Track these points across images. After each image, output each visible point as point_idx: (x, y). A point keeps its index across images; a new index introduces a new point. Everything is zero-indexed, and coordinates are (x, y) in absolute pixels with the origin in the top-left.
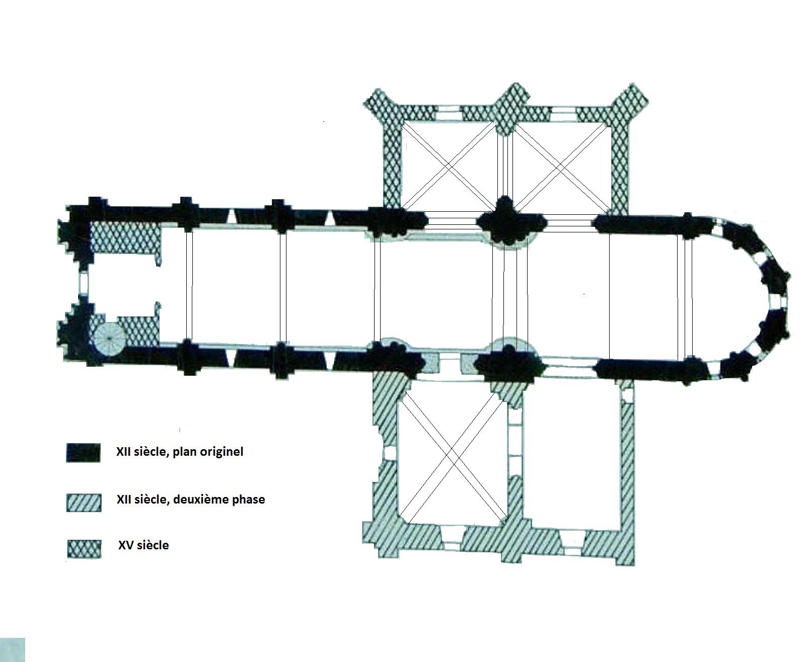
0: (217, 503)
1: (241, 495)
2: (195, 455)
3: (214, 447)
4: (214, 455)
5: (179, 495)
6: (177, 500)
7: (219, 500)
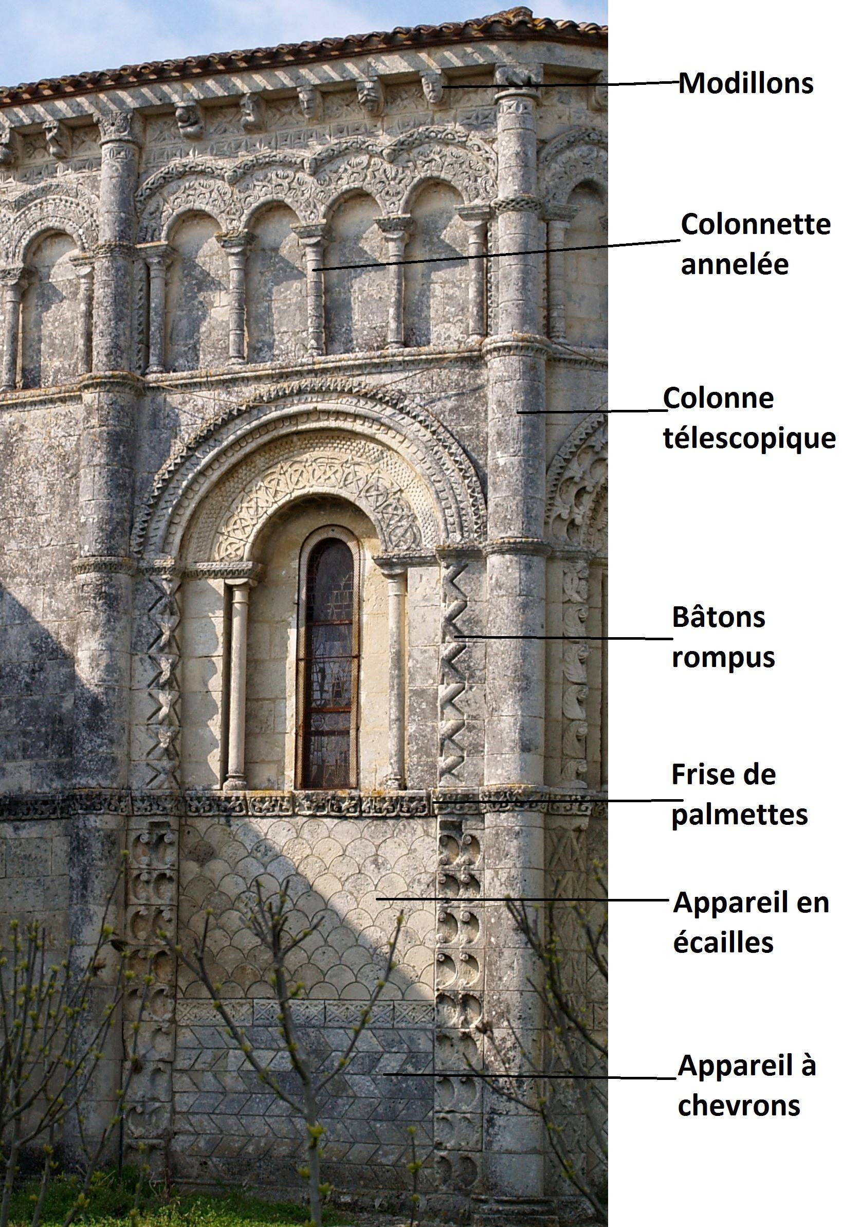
0: (714, 665)
1: (799, 452)
2: (826, 910)
3: (702, 765)
4: (723, 665)
5: (756, 764)
6: (751, 776)
7: (731, 815)
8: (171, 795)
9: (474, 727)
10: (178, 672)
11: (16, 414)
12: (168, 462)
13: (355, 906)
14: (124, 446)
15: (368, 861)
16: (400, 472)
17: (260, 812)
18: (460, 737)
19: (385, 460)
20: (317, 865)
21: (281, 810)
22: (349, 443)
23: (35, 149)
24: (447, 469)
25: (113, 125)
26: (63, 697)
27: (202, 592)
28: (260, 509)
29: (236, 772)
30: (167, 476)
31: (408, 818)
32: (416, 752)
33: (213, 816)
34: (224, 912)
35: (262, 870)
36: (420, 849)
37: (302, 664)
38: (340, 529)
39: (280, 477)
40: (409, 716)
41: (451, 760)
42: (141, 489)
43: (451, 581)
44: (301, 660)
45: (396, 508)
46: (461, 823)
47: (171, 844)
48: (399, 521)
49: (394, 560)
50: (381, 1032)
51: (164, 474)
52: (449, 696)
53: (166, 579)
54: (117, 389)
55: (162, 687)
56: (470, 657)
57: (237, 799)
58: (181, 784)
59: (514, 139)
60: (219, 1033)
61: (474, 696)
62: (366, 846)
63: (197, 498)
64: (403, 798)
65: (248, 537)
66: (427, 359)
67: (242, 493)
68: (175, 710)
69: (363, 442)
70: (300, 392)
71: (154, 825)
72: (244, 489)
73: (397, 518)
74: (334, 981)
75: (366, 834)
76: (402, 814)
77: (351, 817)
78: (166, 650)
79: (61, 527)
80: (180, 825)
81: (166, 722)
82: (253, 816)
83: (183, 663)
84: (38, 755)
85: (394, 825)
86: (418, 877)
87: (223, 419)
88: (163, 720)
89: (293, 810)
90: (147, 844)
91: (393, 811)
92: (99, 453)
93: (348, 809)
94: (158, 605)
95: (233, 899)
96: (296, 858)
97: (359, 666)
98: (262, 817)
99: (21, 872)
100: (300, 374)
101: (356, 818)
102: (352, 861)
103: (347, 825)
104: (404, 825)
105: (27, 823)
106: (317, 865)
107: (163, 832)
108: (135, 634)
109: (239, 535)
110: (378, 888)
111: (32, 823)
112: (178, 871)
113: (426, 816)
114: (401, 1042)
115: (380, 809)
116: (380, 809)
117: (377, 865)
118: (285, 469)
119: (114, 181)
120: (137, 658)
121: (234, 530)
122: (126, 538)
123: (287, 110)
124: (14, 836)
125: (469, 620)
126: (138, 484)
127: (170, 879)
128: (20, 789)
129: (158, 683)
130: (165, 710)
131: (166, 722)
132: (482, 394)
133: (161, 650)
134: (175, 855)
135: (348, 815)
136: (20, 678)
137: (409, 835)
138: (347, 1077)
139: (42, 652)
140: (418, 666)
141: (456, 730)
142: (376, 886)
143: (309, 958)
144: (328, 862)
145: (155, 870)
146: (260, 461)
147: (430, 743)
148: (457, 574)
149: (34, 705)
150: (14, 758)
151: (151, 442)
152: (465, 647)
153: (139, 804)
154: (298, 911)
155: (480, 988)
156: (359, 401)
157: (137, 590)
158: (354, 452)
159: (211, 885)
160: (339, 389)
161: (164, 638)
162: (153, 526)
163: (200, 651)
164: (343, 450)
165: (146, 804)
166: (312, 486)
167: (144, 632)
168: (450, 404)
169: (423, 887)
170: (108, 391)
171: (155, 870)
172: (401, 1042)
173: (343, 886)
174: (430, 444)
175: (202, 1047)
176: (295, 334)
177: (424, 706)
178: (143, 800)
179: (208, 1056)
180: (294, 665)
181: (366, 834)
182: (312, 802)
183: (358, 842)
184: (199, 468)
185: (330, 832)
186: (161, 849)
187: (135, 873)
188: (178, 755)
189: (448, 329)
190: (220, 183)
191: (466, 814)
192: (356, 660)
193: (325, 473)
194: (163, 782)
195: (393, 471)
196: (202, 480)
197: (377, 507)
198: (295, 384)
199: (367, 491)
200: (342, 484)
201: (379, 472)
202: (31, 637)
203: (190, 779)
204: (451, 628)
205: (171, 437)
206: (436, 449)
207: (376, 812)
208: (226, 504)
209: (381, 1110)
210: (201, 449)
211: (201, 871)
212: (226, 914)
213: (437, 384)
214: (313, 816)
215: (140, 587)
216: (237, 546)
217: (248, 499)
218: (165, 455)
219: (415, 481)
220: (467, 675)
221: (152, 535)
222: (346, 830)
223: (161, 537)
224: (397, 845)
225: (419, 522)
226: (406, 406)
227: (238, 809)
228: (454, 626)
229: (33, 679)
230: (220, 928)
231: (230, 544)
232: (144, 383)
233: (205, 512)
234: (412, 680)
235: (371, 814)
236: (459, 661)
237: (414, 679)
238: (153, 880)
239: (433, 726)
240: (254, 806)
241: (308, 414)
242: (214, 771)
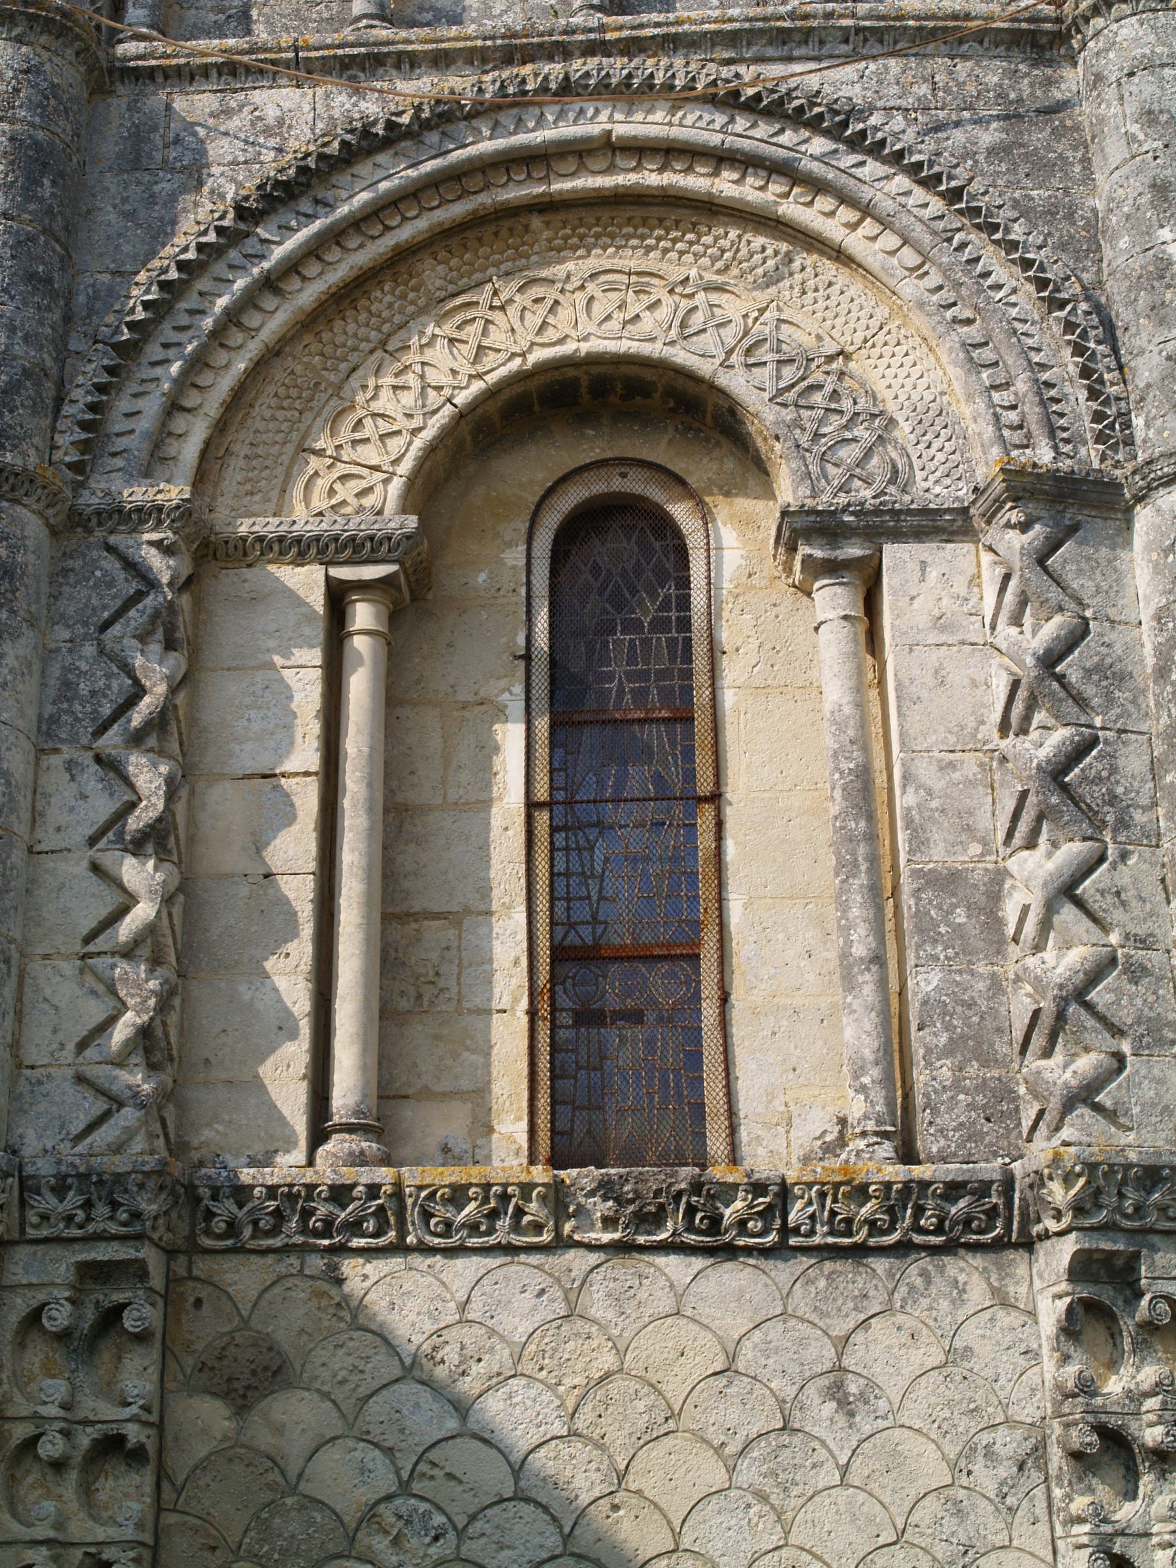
8: (161, 1171)
9: (1144, 969)
10: (180, 808)
12: (180, 241)
13: (775, 1539)
14: (54, 183)
15: (811, 1390)
16: (844, 307)
17: (446, 1234)
18: (1110, 997)
19: (798, 277)
20: (641, 1405)
21: (516, 1228)
22: (690, 236)
24: (999, 287)
27: (256, 599)
28: (432, 393)
29: (357, 1113)
30: (173, 274)
31: (934, 1250)
32: (949, 1051)
33: (287, 1249)
35: (452, 1424)
36: (984, 1350)
38: (646, 473)
39: (491, 315)
40: (919, 946)
41: (1086, 1064)
42: (91, 312)
43: (1041, 561)
44: (540, 805)
45: (835, 395)
46: (1136, 1256)
47: (142, 1338)
48: (846, 427)
49: (847, 518)
51: (164, 271)
52: (1067, 873)
53: (158, 544)
54: (44, 39)
55: (137, 847)
56: (1113, 770)
57: (373, 1190)
58: (178, 1148)
61: (1136, 881)
62: (802, 1342)
63: (254, 348)
64: (924, 1185)
65: (396, 462)
66: (920, 29)
67: (379, 354)
68: (170, 915)
69: (733, 234)
70: (567, 89)
72: (383, 344)
73: (836, 421)
75: (801, 1301)
76: (918, 1239)
77: (749, 1251)
78: (152, 741)
80: (171, 1280)
81: (145, 951)
82: (425, 1249)
83: (192, 793)
85: (890, 1274)
86: (986, 1438)
87: (344, 143)
88: (137, 942)
89: (558, 1229)
90: (64, 1336)
91: (891, 1229)
93: (742, 1224)
94: (132, 613)
95: (350, 1520)
96: (568, 1382)
97: (720, 825)
98: (450, 1252)
100: (561, 51)
101: (765, 1252)
102: (759, 1390)
104: (924, 1273)
106: (641, 1405)
107: (119, 1297)
108: (52, 692)
109: (370, 454)
110: (854, 1478)
112: (160, 1426)
113: (999, 1245)
115: (849, 1221)
116: (849, 1221)
118: (504, 296)
120: (56, 760)
121: (355, 443)
122: (46, 423)
125: (1098, 668)
126: (82, 299)
127: (137, 1456)
129: (121, 835)
130: (143, 912)
131: (145, 951)
132: (1069, 123)
133: (136, 739)
134: (153, 1373)
135: (741, 1242)
137: (945, 1305)
140: (934, 804)
141: (1094, 976)
142: (845, 1470)
144: (675, 1391)
145: (86, 1423)
146: (433, 274)
147: (989, 1024)
148: (1053, 546)
151: (125, 200)
152: (1095, 741)
153: (48, 1202)
154: (580, 1557)
156: (732, 120)
157: (65, 572)
158: (705, 261)
159: (275, 1476)
160: (679, 83)
161: (146, 706)
162: (124, 404)
163: (248, 759)
164: (673, 255)
165: (73, 1199)
166: (585, 339)
167: (84, 688)
168: (989, 137)
169: (1005, 1471)
170: (19, 40)
171: (86, 1423)
173: (731, 1470)
174: (941, 225)
177: (960, 916)
178: (60, 1190)
180: (520, 820)
182: (620, 1201)
183: (775, 1330)
184: (266, 265)
185: (679, 1298)
186: (106, 1356)
187: (20, 1432)
188: (171, 1059)
191: (1152, 1231)
192: (708, 810)
193: (622, 306)
194: (130, 1134)
195: (821, 304)
196: (180, 423)
197: (781, 392)
199: (748, 352)
200: (673, 333)
201: (779, 309)
203: (207, 1134)
204: (1055, 685)
205: (184, 189)
206: (958, 238)
207: (831, 1233)
208: (332, 377)
210: (275, 220)
211: (240, 1430)
213: (947, 90)
214: (623, 1248)
215: (77, 564)
216: (364, 484)
217: (398, 366)
218: (164, 230)
219: (892, 326)
220: (1110, 818)
221: (117, 428)
223: (146, 435)
224: (904, 1337)
225: (904, 431)
226: (876, 129)
227: (370, 1225)
228: (1061, 679)
231: (343, 478)
232: (113, 59)
233: (271, 389)
234: (919, 843)
235: (817, 1240)
236: (1084, 779)
237: (925, 842)
238: (78, 1458)
239: (994, 975)
240: (427, 1215)
242: (286, 1112)
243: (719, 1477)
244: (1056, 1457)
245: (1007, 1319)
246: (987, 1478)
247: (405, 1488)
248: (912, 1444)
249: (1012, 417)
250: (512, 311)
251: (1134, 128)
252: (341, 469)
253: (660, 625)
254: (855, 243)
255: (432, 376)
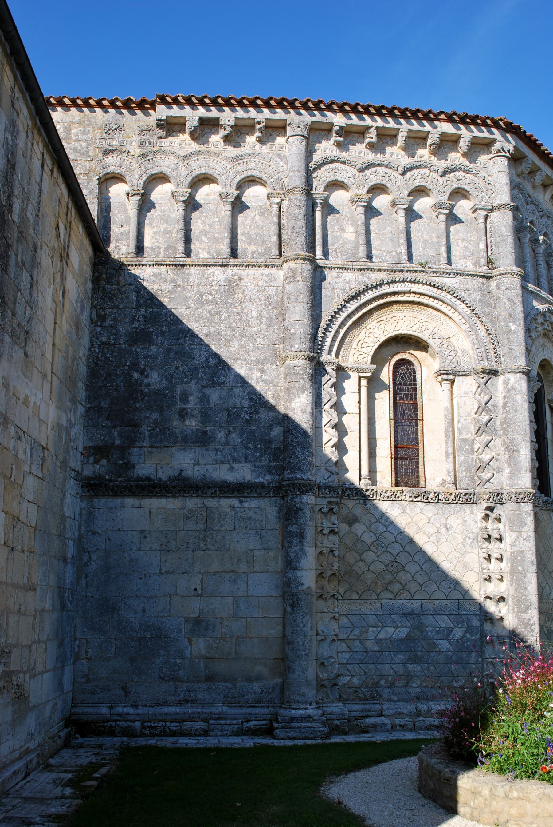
11: (236, 270)
23: (241, 134)
25: (299, 127)
26: (271, 429)
32: (465, 470)
34: (364, 552)
35: (385, 529)
37: (392, 421)
50: (453, 617)
59: (505, 176)
60: (363, 619)
62: (440, 518)
71: (330, 503)
74: (427, 589)
79: (267, 335)
84: (255, 461)
92: (302, 296)
99: (245, 526)
103: (430, 507)
105: (249, 499)
110: (448, 540)
111: (252, 499)
114: (463, 621)
117: (447, 528)
119: (300, 156)
123: (385, 141)
124: (239, 506)
125: (493, 406)
128: (244, 479)
136: (242, 416)
138: (435, 641)
139: (256, 403)
143: (413, 577)
144: (420, 525)
149: (252, 432)
150: (240, 462)
155: (506, 593)
172: (463, 621)
175: (353, 626)
176: (389, 252)
177: (467, 447)
179: (357, 631)
181: (440, 512)
183: (436, 516)
189: (466, 262)
190: (352, 169)
198: (401, 276)
202: (249, 394)
209: (454, 658)
212: (365, 554)
222: (430, 509)
225: (459, 354)
229: (251, 417)
230: (362, 560)
234: (460, 433)
241: (404, 293)
243: (427, 539)
244: (480, 538)
245: (472, 516)
246: (469, 541)
247: (378, 540)
248: (457, 535)
249: (480, 355)
250: (390, 322)
251: (506, 301)
252: (359, 353)
253: (410, 384)
254: (454, 316)
255: (376, 336)
